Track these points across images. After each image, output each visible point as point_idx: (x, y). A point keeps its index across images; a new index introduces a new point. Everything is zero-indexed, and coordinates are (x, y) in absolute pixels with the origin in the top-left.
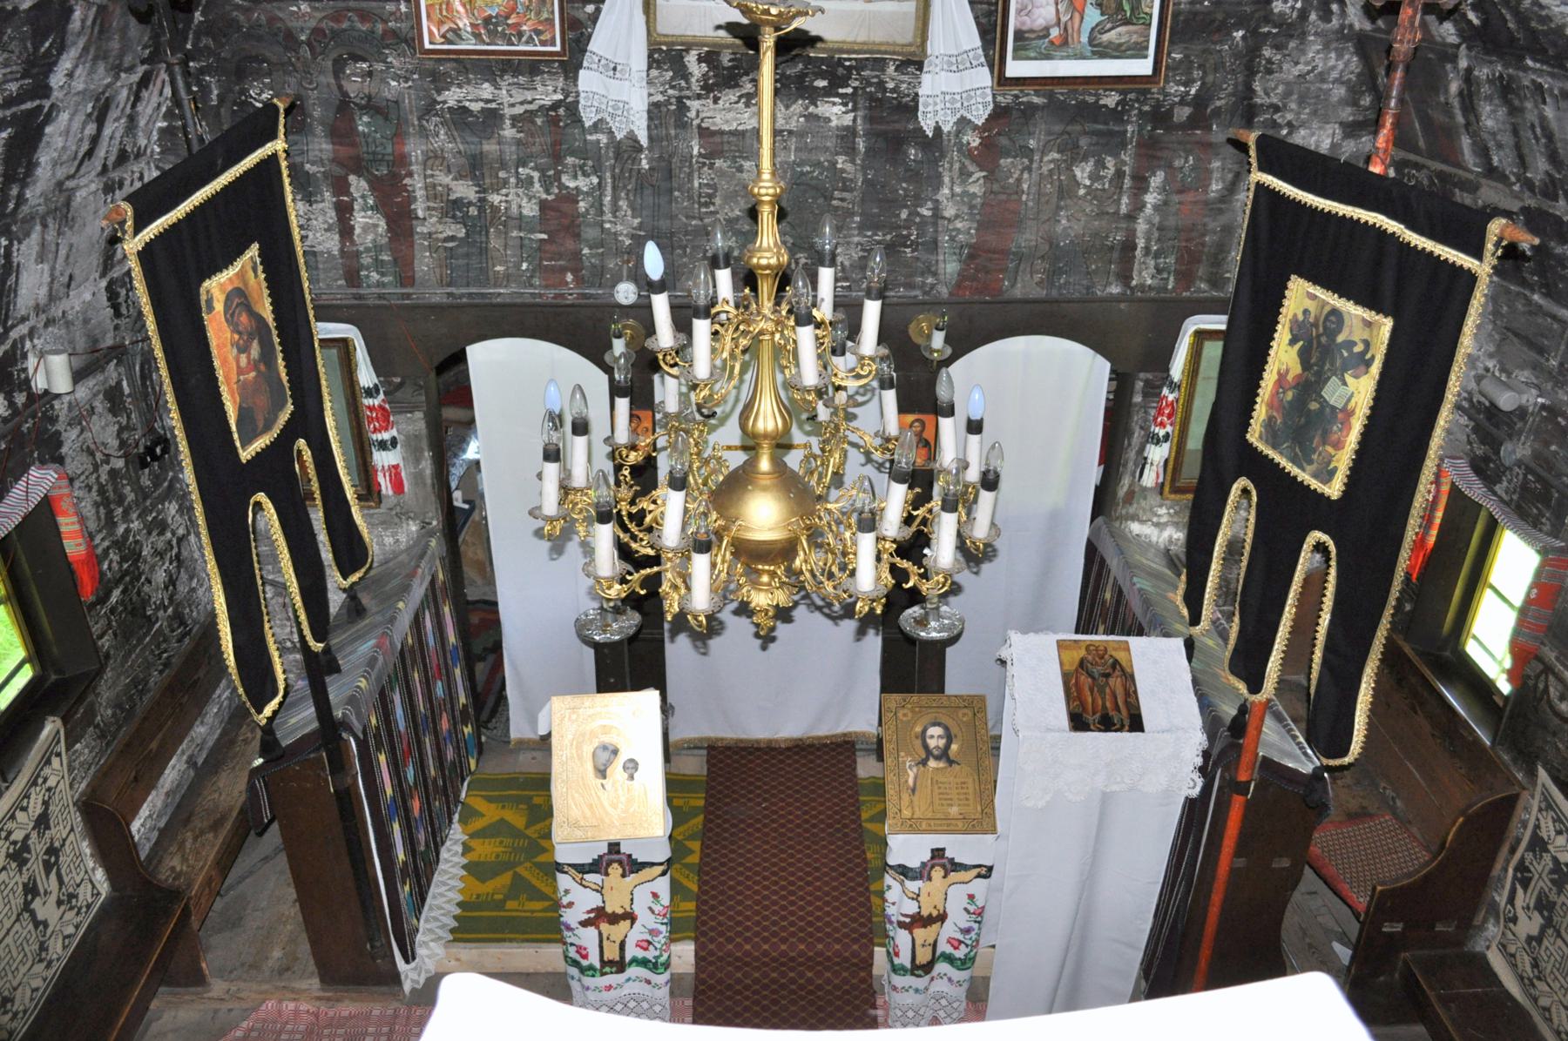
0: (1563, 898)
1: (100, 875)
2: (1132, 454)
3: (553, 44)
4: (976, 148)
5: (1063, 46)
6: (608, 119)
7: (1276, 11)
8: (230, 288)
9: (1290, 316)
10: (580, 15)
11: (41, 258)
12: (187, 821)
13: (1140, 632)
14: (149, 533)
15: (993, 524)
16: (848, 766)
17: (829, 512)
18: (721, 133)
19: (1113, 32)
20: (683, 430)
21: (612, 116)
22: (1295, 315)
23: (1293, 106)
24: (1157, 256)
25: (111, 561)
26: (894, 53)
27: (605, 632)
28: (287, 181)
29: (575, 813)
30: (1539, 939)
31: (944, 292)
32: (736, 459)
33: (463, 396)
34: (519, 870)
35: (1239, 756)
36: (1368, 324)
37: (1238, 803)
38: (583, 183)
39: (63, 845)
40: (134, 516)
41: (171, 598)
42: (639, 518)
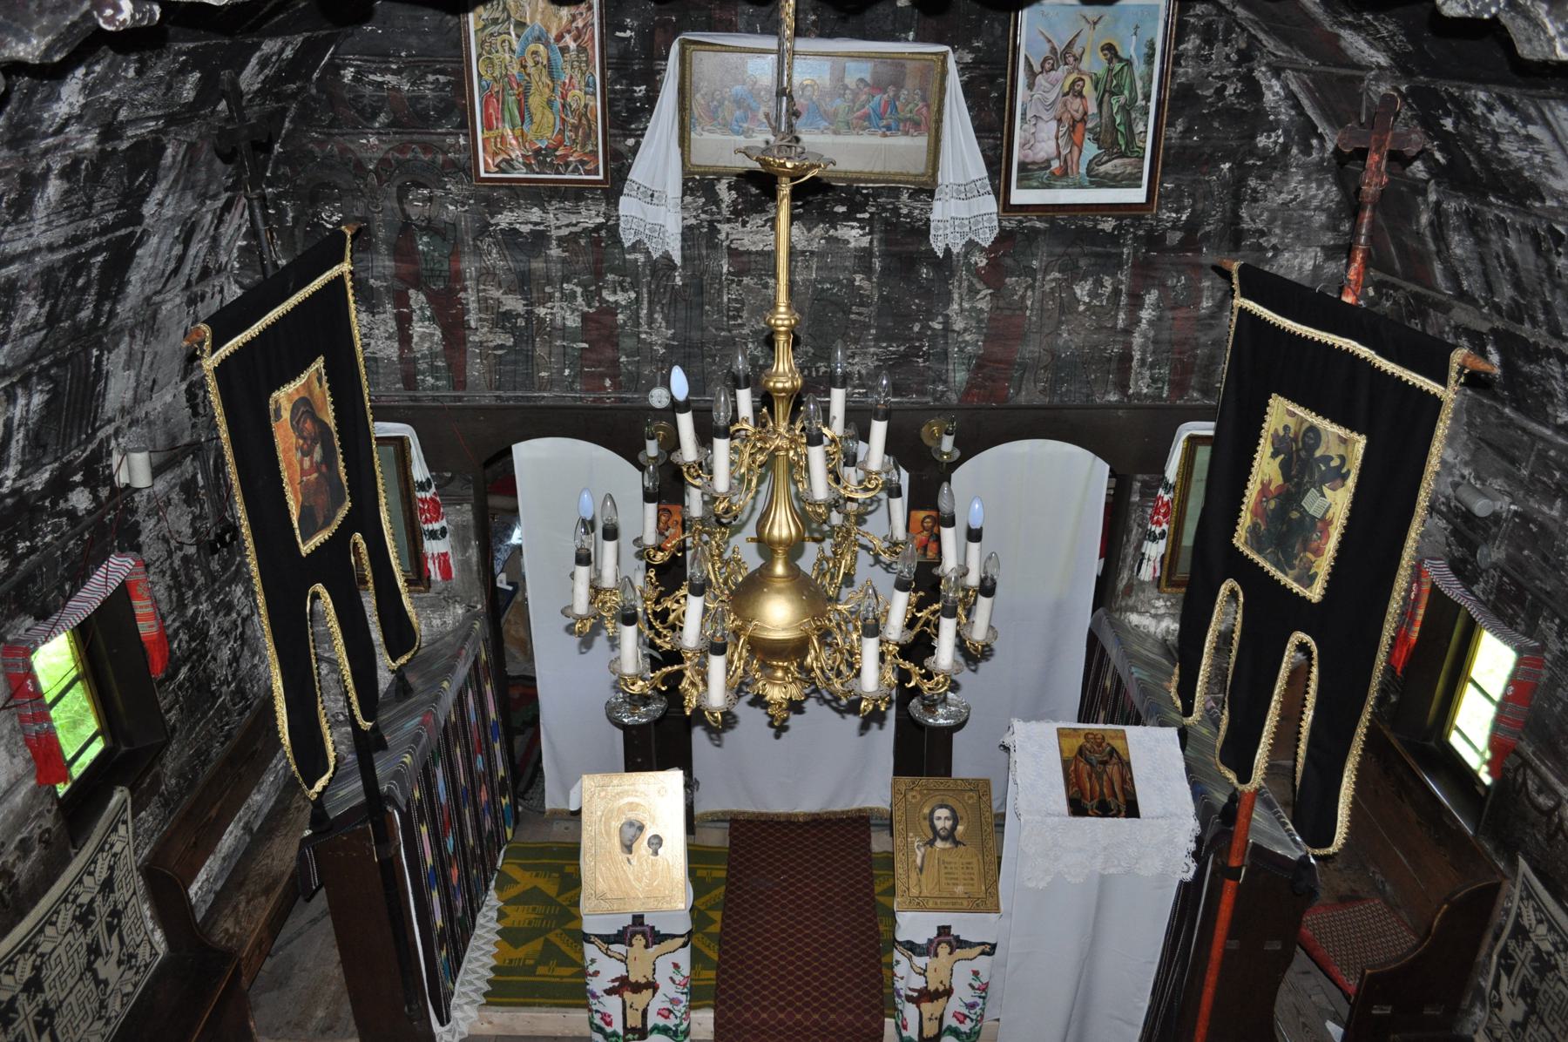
0: (1545, 986)
1: (158, 936)
2: (1131, 550)
3: (597, 173)
4: (983, 268)
5: (1062, 177)
6: (646, 241)
7: (1260, 145)
8: (296, 398)
9: (1272, 431)
10: (620, 147)
11: (128, 366)
12: (241, 884)
13: (1138, 721)
14: (217, 614)
15: (990, 627)
16: (864, 840)
17: (840, 612)
18: (749, 253)
19: (1110, 164)
20: (706, 532)
21: (650, 238)
22: (1276, 430)
23: (1278, 231)
24: (1152, 367)
25: (180, 641)
26: (907, 182)
27: (633, 715)
28: (350, 292)
29: (602, 886)
30: (1523, 1025)
31: (954, 398)
32: (753, 561)
33: (508, 486)
34: (551, 936)
35: (1230, 843)
36: (1344, 441)
37: (1230, 887)
38: (621, 298)
39: (126, 907)
40: (204, 598)
41: (234, 675)
42: (663, 616)
